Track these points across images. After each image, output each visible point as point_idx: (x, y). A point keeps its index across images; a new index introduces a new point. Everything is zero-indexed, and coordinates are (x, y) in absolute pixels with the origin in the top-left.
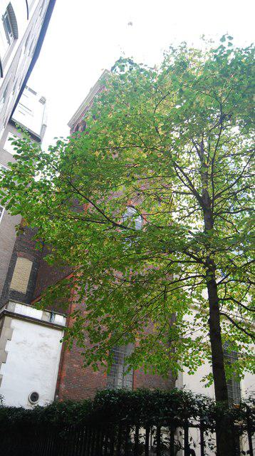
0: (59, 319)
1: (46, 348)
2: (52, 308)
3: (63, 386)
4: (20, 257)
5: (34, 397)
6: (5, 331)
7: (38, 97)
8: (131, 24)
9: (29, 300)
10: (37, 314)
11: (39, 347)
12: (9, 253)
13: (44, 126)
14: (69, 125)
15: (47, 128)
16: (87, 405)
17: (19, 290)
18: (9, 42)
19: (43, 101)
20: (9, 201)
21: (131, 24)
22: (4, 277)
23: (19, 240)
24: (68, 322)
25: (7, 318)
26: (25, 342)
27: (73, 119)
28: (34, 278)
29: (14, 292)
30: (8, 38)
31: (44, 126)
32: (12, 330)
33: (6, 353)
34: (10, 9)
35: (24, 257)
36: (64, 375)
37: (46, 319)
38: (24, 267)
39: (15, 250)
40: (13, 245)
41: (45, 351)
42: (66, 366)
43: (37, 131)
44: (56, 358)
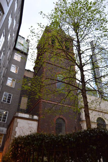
0: (36, 117)
6: (15, 124)
10: (27, 116)
12: (19, 96)
22: (17, 104)
25: (15, 119)
37: (31, 118)
38: (25, 100)
39: (21, 94)
40: (20, 93)
43: (26, 52)
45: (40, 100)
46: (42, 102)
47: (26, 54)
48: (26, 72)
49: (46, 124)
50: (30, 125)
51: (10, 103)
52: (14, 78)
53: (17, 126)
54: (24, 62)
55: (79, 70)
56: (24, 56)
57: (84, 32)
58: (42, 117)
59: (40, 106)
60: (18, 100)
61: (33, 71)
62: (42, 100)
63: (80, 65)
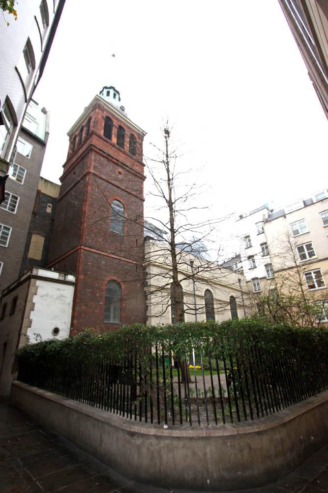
0: (71, 278)
1: (62, 298)
2: (64, 271)
3: (75, 321)
4: (35, 234)
5: (56, 331)
6: (32, 290)
7: (40, 107)
8: (114, 56)
9: (46, 266)
10: (55, 275)
11: (58, 298)
12: (26, 231)
13: (47, 134)
14: (68, 134)
15: (50, 135)
16: (61, 341)
17: (36, 258)
18: (29, 72)
19: (44, 111)
20: (304, 278)
21: (114, 56)
22: (23, 249)
23: (32, 222)
24: (77, 280)
25: (32, 280)
26: (47, 295)
27: (72, 130)
28: (46, 249)
29: (31, 260)
30: (28, 69)
31: (47, 134)
32: (37, 288)
33: (34, 304)
34: (29, 44)
35: (38, 234)
36: (76, 314)
37: (62, 278)
38: (38, 242)
39: (30, 229)
40: (28, 226)
41: (62, 300)
42: (77, 309)
43: (41, 136)
44: (70, 304)
45: (79, 247)
46: (82, 250)
47: (40, 143)
48: (41, 183)
49: (90, 290)
50: (62, 292)
51: (7, 246)
52: (16, 193)
53: (36, 294)
54: (37, 160)
55: (181, 281)
56: (39, 147)
57: (192, 267)
58: (82, 277)
59: (80, 257)
60: (23, 241)
61: (60, 184)
62: (82, 247)
63: (169, 201)
